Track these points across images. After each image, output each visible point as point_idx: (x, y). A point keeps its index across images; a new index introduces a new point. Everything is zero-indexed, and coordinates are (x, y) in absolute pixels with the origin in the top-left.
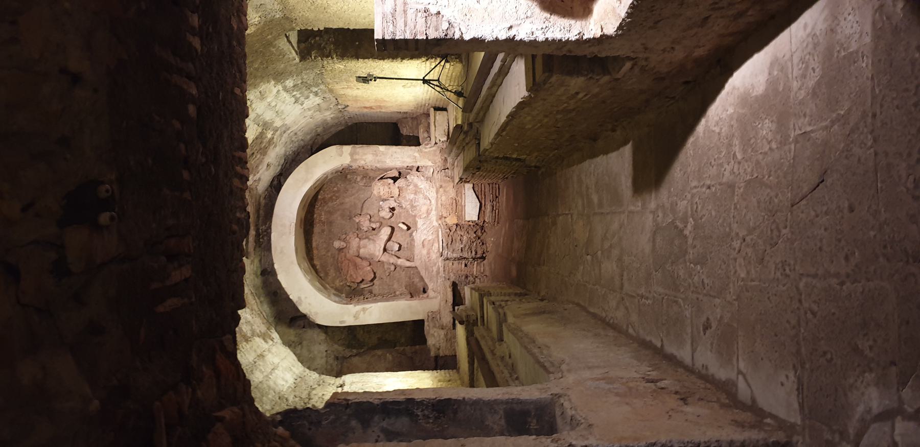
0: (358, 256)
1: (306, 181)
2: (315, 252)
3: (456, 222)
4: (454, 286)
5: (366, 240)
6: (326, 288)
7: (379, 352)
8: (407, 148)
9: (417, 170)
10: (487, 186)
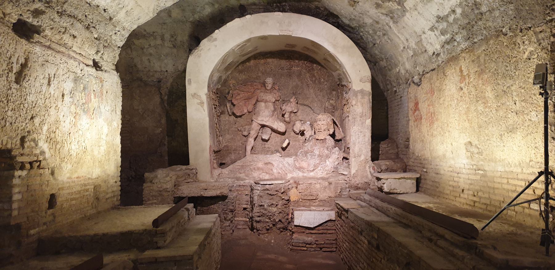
0: (257, 101)
1: (335, 46)
2: (262, 61)
3: (293, 199)
4: (223, 198)
5: (273, 109)
6: (227, 69)
7: (163, 121)
8: (369, 148)
9: (345, 158)
10: (334, 237)
